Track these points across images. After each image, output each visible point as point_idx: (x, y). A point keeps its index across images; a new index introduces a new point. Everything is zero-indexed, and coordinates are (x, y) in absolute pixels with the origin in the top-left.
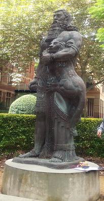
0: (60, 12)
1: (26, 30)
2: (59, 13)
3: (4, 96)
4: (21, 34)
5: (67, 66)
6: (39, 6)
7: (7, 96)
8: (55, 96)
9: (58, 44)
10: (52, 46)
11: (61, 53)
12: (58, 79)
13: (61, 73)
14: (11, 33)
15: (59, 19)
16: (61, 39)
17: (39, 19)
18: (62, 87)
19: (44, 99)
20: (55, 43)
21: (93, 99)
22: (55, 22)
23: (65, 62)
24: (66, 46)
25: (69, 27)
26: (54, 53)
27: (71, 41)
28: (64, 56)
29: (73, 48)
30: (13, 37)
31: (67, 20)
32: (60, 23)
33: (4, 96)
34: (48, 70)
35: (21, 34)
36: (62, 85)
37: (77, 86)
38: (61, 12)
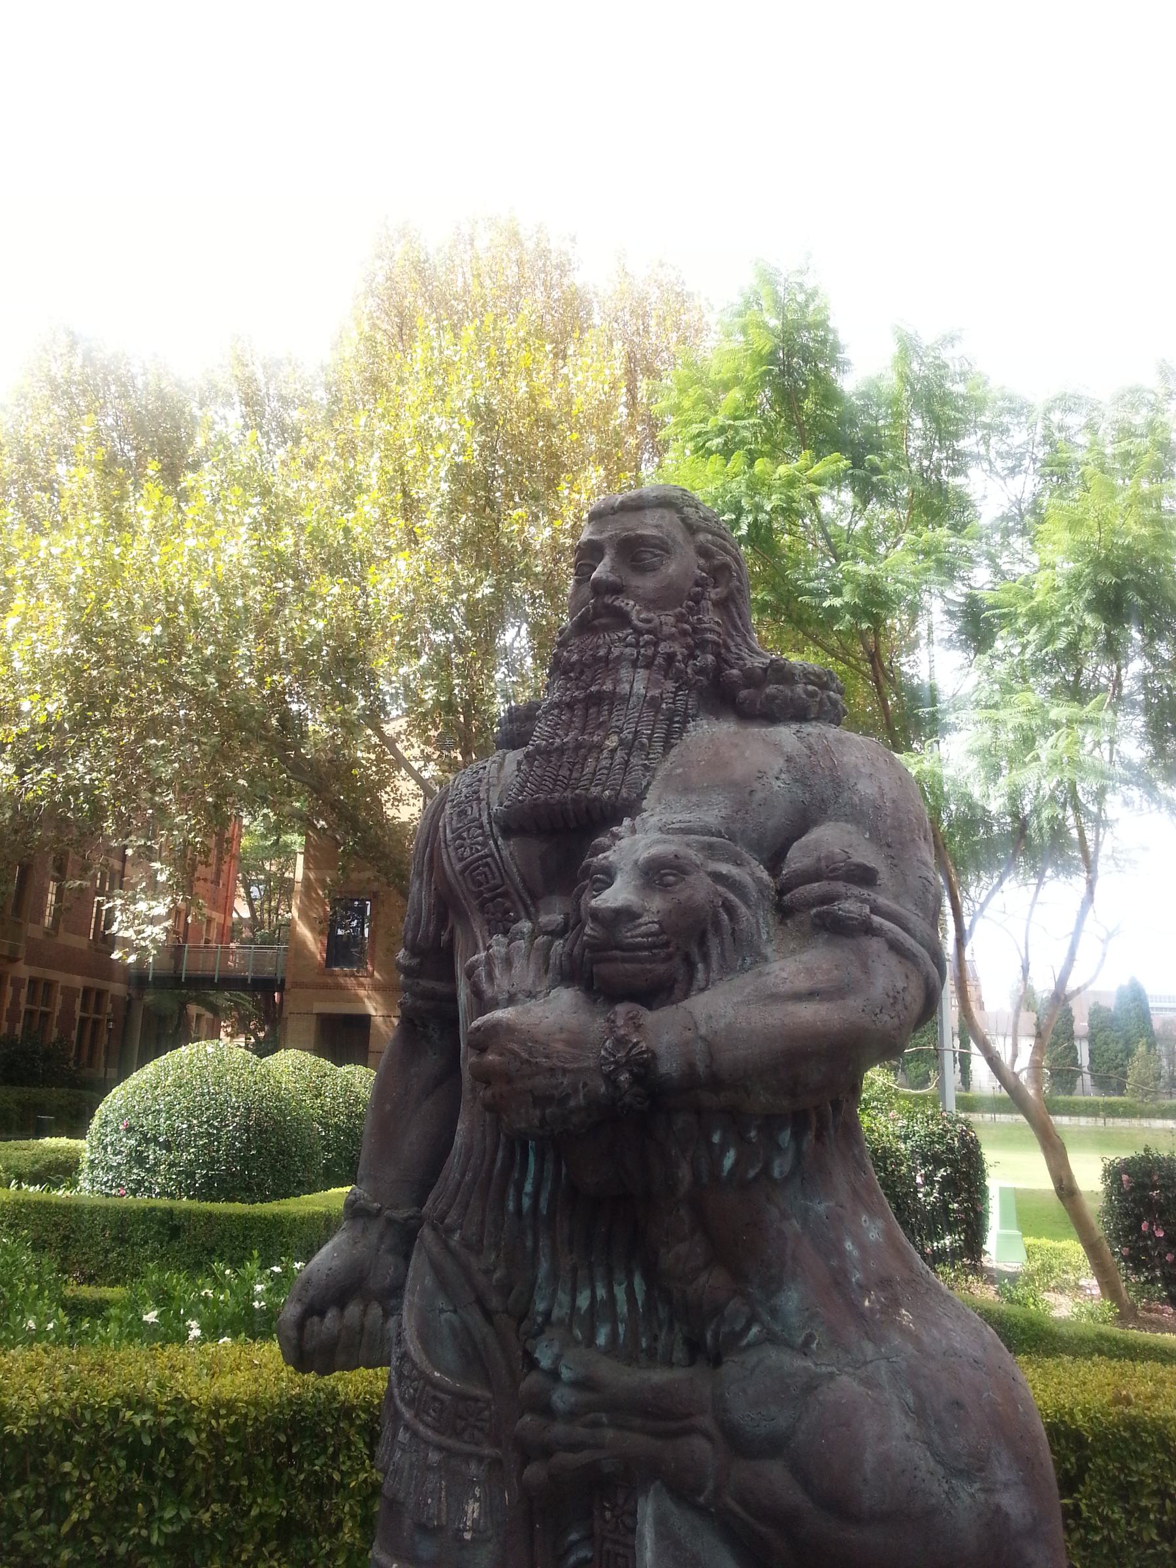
1: (206, 665)
2: (649, 525)
3: (67, 1011)
4: (173, 687)
6: (281, 547)
7: (84, 1007)
9: (699, 889)
10: (626, 915)
14: (123, 681)
15: (647, 584)
17: (275, 613)
20: (656, 874)
25: (753, 679)
26: (656, 993)
29: (895, 947)
30: (129, 702)
31: (722, 605)
33: (67, 1011)
35: (173, 687)
36: (774, 1446)
37: (972, 1468)
38: (669, 518)
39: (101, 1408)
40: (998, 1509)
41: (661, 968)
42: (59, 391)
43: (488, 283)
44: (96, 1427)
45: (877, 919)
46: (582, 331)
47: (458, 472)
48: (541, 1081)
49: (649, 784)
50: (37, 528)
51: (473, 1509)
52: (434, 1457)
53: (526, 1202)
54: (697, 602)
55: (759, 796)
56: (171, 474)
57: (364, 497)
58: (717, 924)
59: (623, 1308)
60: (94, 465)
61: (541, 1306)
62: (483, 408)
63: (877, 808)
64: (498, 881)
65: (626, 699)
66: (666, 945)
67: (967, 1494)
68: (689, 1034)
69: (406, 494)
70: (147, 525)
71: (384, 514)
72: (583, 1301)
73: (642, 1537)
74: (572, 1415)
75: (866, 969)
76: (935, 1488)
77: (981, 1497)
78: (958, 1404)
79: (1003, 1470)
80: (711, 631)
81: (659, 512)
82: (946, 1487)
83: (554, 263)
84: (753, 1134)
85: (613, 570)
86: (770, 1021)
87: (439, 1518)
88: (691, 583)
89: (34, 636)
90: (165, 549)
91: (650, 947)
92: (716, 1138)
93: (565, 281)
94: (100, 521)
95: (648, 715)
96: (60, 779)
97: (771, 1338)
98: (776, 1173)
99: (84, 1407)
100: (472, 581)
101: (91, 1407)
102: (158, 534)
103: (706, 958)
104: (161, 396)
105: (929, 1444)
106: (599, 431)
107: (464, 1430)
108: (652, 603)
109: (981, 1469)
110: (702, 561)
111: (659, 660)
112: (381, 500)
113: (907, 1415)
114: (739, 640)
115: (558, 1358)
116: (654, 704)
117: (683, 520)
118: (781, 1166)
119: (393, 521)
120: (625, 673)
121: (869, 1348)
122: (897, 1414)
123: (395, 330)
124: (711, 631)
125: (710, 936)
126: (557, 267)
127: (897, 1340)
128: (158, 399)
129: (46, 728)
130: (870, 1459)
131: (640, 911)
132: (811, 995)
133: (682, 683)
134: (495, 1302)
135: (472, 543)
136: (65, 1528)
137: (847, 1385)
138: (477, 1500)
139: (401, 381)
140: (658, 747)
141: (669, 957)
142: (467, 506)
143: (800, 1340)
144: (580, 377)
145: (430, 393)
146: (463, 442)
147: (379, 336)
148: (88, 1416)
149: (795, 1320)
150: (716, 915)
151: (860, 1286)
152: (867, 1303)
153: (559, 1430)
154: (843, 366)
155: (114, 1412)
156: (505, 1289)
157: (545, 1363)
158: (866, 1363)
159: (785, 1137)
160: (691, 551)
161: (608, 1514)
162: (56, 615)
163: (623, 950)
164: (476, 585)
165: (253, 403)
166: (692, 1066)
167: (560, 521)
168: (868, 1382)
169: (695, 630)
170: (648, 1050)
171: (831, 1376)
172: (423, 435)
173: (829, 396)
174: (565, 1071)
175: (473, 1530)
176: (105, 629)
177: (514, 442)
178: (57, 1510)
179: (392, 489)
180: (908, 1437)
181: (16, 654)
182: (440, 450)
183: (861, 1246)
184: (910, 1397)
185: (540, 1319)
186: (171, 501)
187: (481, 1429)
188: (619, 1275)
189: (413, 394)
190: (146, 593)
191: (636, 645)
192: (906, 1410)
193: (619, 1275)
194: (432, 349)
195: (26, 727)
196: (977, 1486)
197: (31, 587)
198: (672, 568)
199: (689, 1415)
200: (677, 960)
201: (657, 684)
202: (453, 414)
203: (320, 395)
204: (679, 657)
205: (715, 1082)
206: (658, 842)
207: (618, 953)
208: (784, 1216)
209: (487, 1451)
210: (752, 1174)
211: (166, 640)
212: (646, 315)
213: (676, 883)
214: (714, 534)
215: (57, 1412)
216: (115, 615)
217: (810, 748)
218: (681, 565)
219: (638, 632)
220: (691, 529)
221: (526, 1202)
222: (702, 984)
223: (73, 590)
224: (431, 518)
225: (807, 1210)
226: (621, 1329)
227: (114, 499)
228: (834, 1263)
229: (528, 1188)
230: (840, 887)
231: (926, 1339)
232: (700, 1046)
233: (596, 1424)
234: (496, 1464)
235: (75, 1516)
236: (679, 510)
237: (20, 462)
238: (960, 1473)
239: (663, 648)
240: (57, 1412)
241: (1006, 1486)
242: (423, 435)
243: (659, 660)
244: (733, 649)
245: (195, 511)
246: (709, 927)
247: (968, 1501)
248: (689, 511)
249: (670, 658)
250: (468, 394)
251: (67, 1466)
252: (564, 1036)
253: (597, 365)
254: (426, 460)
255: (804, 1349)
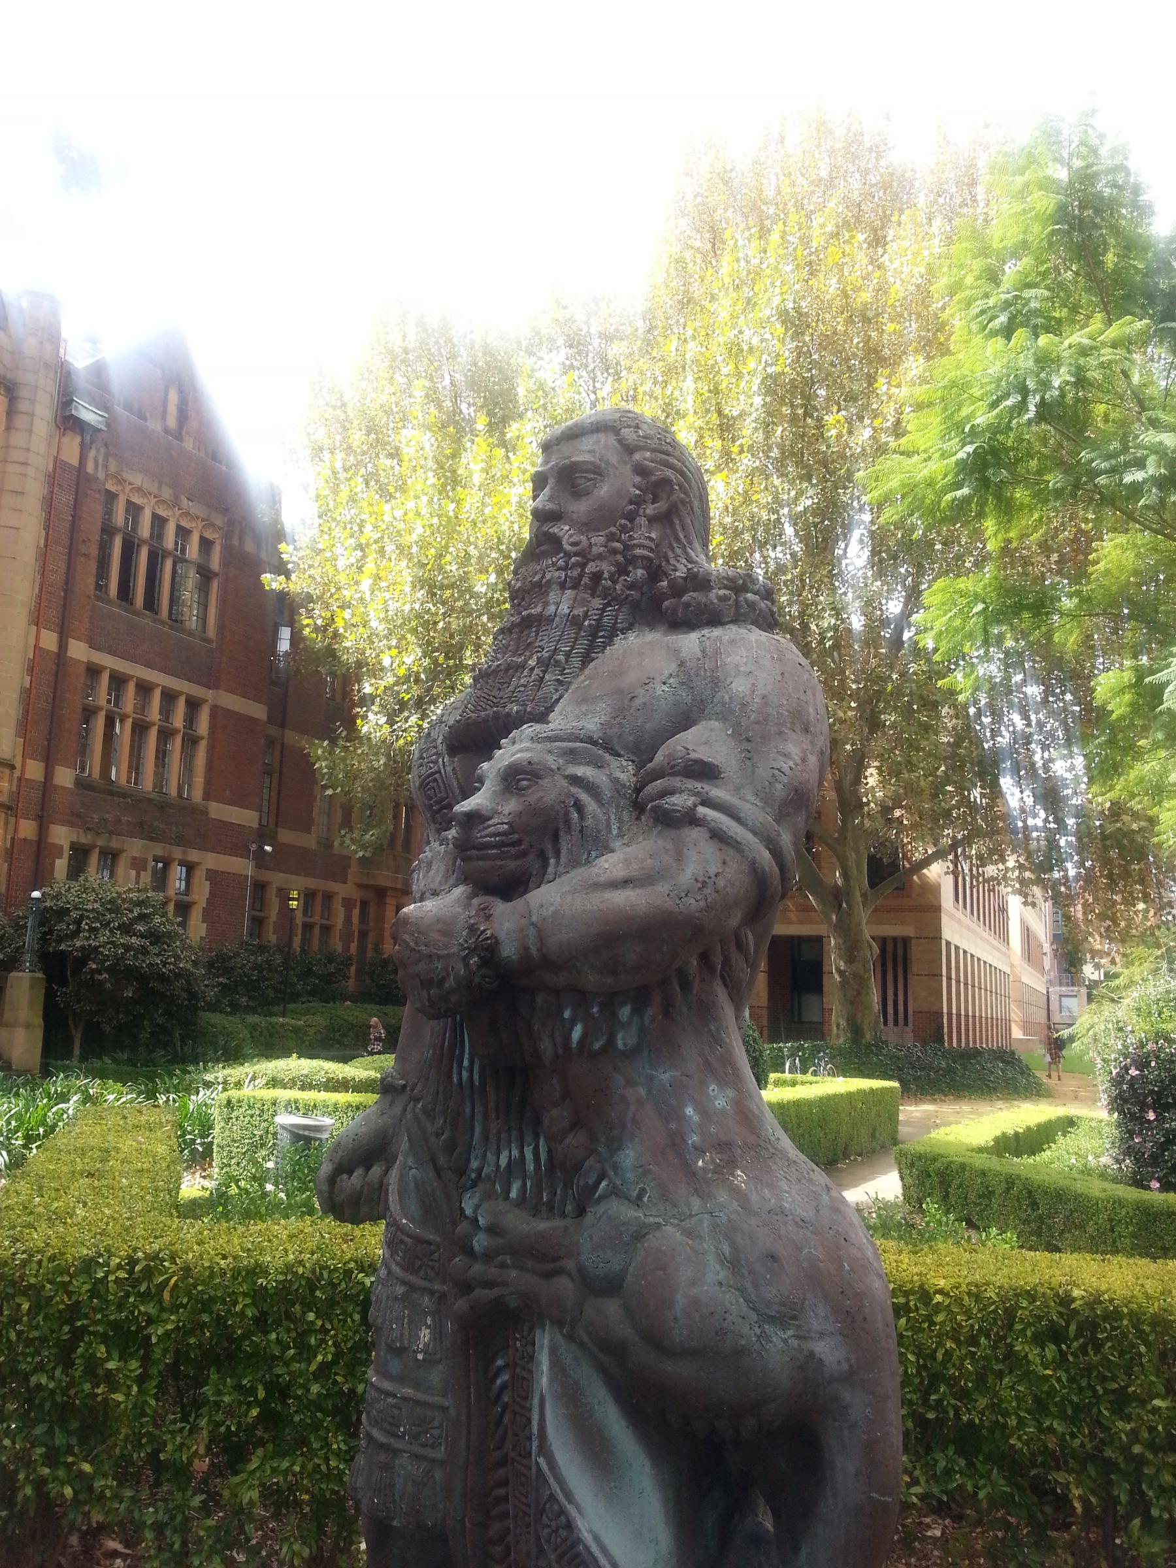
0: (587, 443)
5: (659, 1044)
8: (544, 1379)
9: (550, 791)
11: (565, 900)
12: (570, 1185)
13: (596, 1122)
15: (580, 508)
16: (592, 725)
18: (612, 1307)
19: (436, 1376)
20: (516, 779)
21: (906, 941)
22: (543, 544)
23: (640, 998)
24: (638, 807)
25: (677, 590)
27: (703, 741)
28: (612, 940)
32: (585, 556)
34: (467, 1068)
36: (612, 1286)
37: (787, 1315)
39: (336, 1269)
40: (811, 1355)
41: (513, 865)
42: (398, 360)
43: (800, 180)
44: (331, 1283)
45: (702, 810)
46: (901, 212)
47: (772, 385)
48: (422, 967)
49: (557, 701)
50: (385, 494)
51: (425, 1335)
52: (400, 1290)
53: (465, 1074)
54: (632, 520)
55: (638, 702)
56: (498, 425)
57: (681, 422)
58: (568, 822)
59: (530, 1167)
60: (427, 427)
61: (474, 1164)
62: (792, 313)
63: (745, 705)
64: (444, 795)
65: (550, 620)
66: (519, 842)
67: (779, 1340)
68: (524, 921)
69: (720, 412)
70: (477, 478)
71: (702, 437)
72: (503, 1162)
73: (540, 1363)
74: (488, 1256)
75: (679, 857)
76: (745, 1330)
77: (794, 1343)
78: (773, 1257)
79: (818, 1319)
80: (641, 546)
81: (595, 436)
82: (758, 1331)
83: (867, 145)
84: (595, 1010)
85: (551, 499)
86: (589, 907)
87: (401, 1341)
88: (625, 502)
89: (387, 595)
90: (495, 500)
91: (502, 845)
92: (567, 1014)
93: (883, 162)
94: (434, 480)
95: (571, 632)
96: (426, 725)
97: (615, 1192)
98: (620, 1044)
99: (322, 1268)
100: (793, 493)
101: (328, 1267)
102: (487, 490)
103: (557, 854)
104: (487, 351)
105: (741, 1291)
106: (919, 316)
107: (420, 1269)
108: (587, 526)
109: (795, 1318)
110: (638, 479)
111: (586, 580)
112: (697, 424)
113: (722, 1264)
114: (679, 551)
115: (477, 1207)
116: (575, 622)
117: (620, 441)
118: (623, 1038)
119: (709, 443)
120: (553, 596)
121: (696, 1203)
122: (712, 1260)
123: (709, 246)
124: (641, 546)
125: (561, 834)
126: (870, 150)
127: (723, 1197)
128: (485, 354)
129: (406, 679)
130: (680, 1300)
131: (489, 814)
132: (626, 883)
133: (610, 598)
134: (442, 1160)
135: (793, 454)
136: (313, 1367)
137: (672, 1233)
138: (428, 1327)
139: (713, 298)
140: (576, 662)
141: (524, 854)
142: (783, 416)
143: (635, 1194)
144: (897, 264)
145: (739, 307)
146: (773, 351)
147: (688, 255)
148: (325, 1274)
149: (630, 1176)
150: (567, 813)
151: (696, 1148)
152: (700, 1163)
153: (477, 1268)
154: (1144, 211)
155: (348, 1273)
156: (451, 1147)
157: (469, 1212)
158: (691, 1216)
159: (625, 1012)
160: (627, 470)
161: (518, 1344)
162: (405, 575)
163: (479, 849)
164: (796, 499)
165: (576, 343)
166: (526, 949)
167: (880, 420)
168: (690, 1233)
169: (626, 547)
170: (492, 936)
171: (658, 1226)
172: (736, 351)
173: (1131, 246)
174: (439, 957)
175: (425, 1352)
176: (446, 582)
177: (828, 342)
178: (306, 1352)
179: (708, 411)
180: (720, 1284)
181: (372, 614)
182: (752, 363)
183: (704, 1113)
184: (726, 1249)
185: (473, 1176)
186: (500, 452)
187: (432, 1268)
188: (528, 1138)
189: (723, 308)
190: (481, 544)
191: (565, 569)
192: (722, 1260)
193: (528, 1138)
194: (738, 261)
195: (391, 680)
196: (790, 1332)
197: (382, 551)
198: (604, 491)
199: (557, 1259)
200: (532, 857)
201: (584, 602)
202: (763, 323)
203: (641, 326)
204: (606, 575)
205: (548, 963)
206: (527, 750)
207: (474, 852)
208: (630, 1083)
209: (437, 1287)
210: (597, 1045)
211: (500, 586)
212: (973, 183)
213: (528, 787)
214: (653, 450)
215: (301, 1270)
216: (454, 568)
217: (703, 651)
218: (619, 483)
219: (568, 555)
220: (628, 449)
221: (465, 1074)
222: (551, 877)
223: (414, 549)
224: (749, 432)
225: (652, 1078)
226: (529, 1183)
227: (448, 458)
228: (673, 1126)
229: (466, 1063)
230: (677, 782)
231: (754, 1198)
232: (532, 931)
233: (503, 1266)
234: (442, 1298)
235: (320, 1358)
236: (617, 432)
237: (368, 433)
238: (771, 1320)
239: (591, 568)
240: (301, 1270)
241: (822, 1335)
242: (736, 351)
243: (586, 580)
244: (672, 561)
245: (520, 459)
246: (561, 826)
247: (781, 1345)
248: (625, 432)
249: (597, 577)
250: (777, 301)
251: (311, 1316)
252: (439, 927)
253: (915, 247)
254: (739, 375)
255: (637, 1202)
